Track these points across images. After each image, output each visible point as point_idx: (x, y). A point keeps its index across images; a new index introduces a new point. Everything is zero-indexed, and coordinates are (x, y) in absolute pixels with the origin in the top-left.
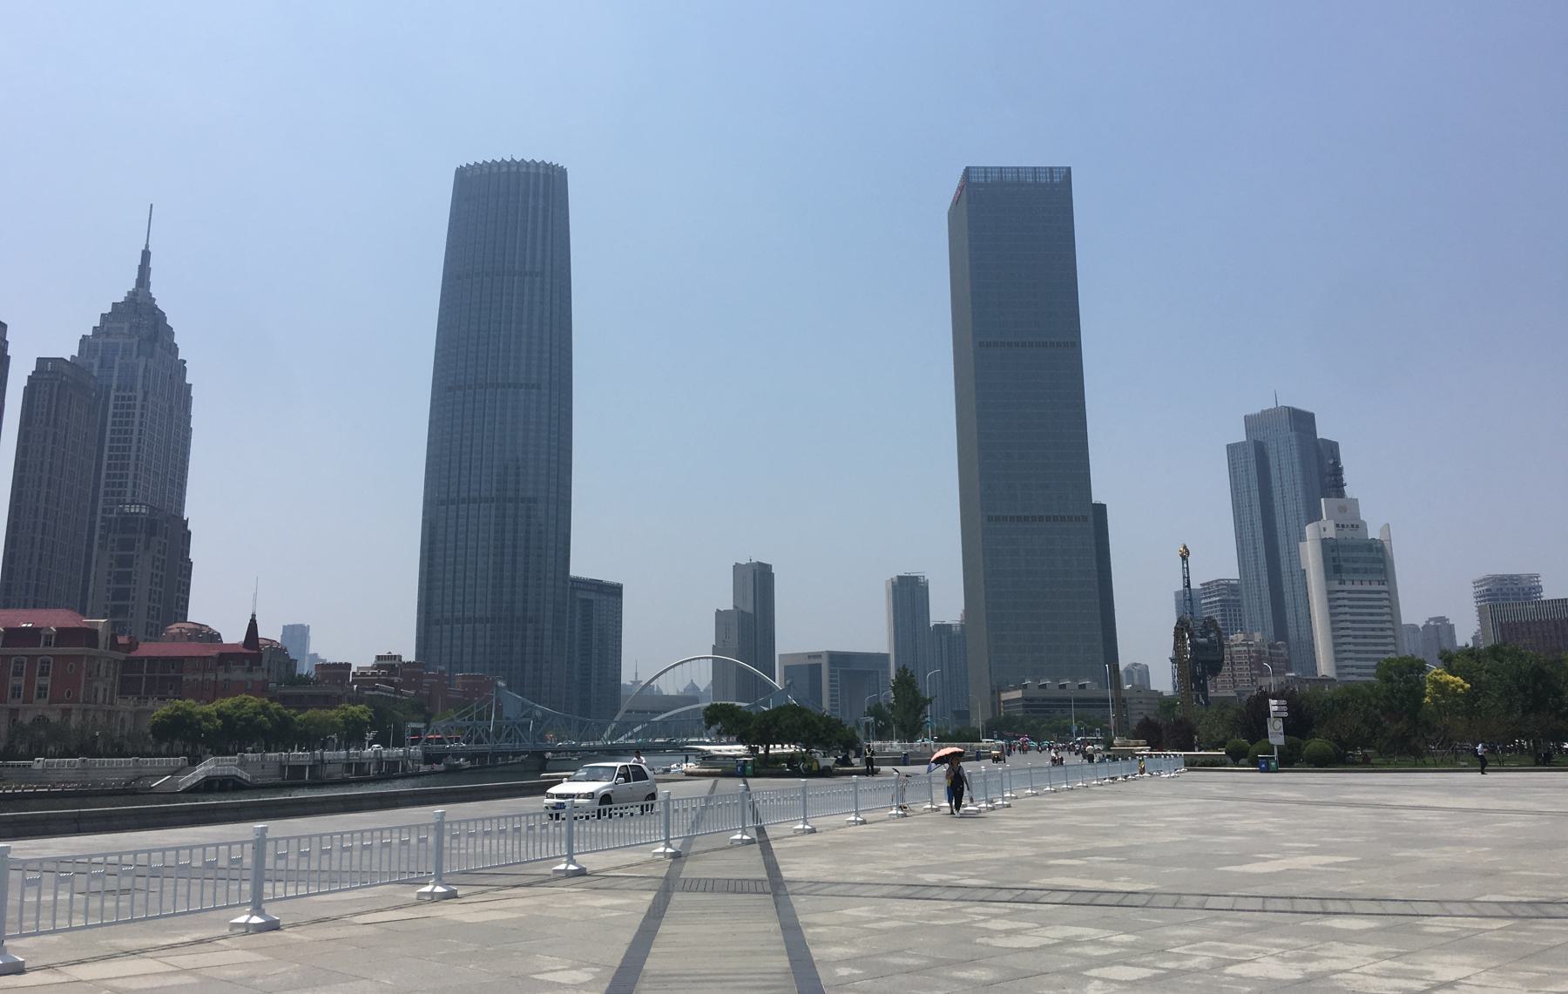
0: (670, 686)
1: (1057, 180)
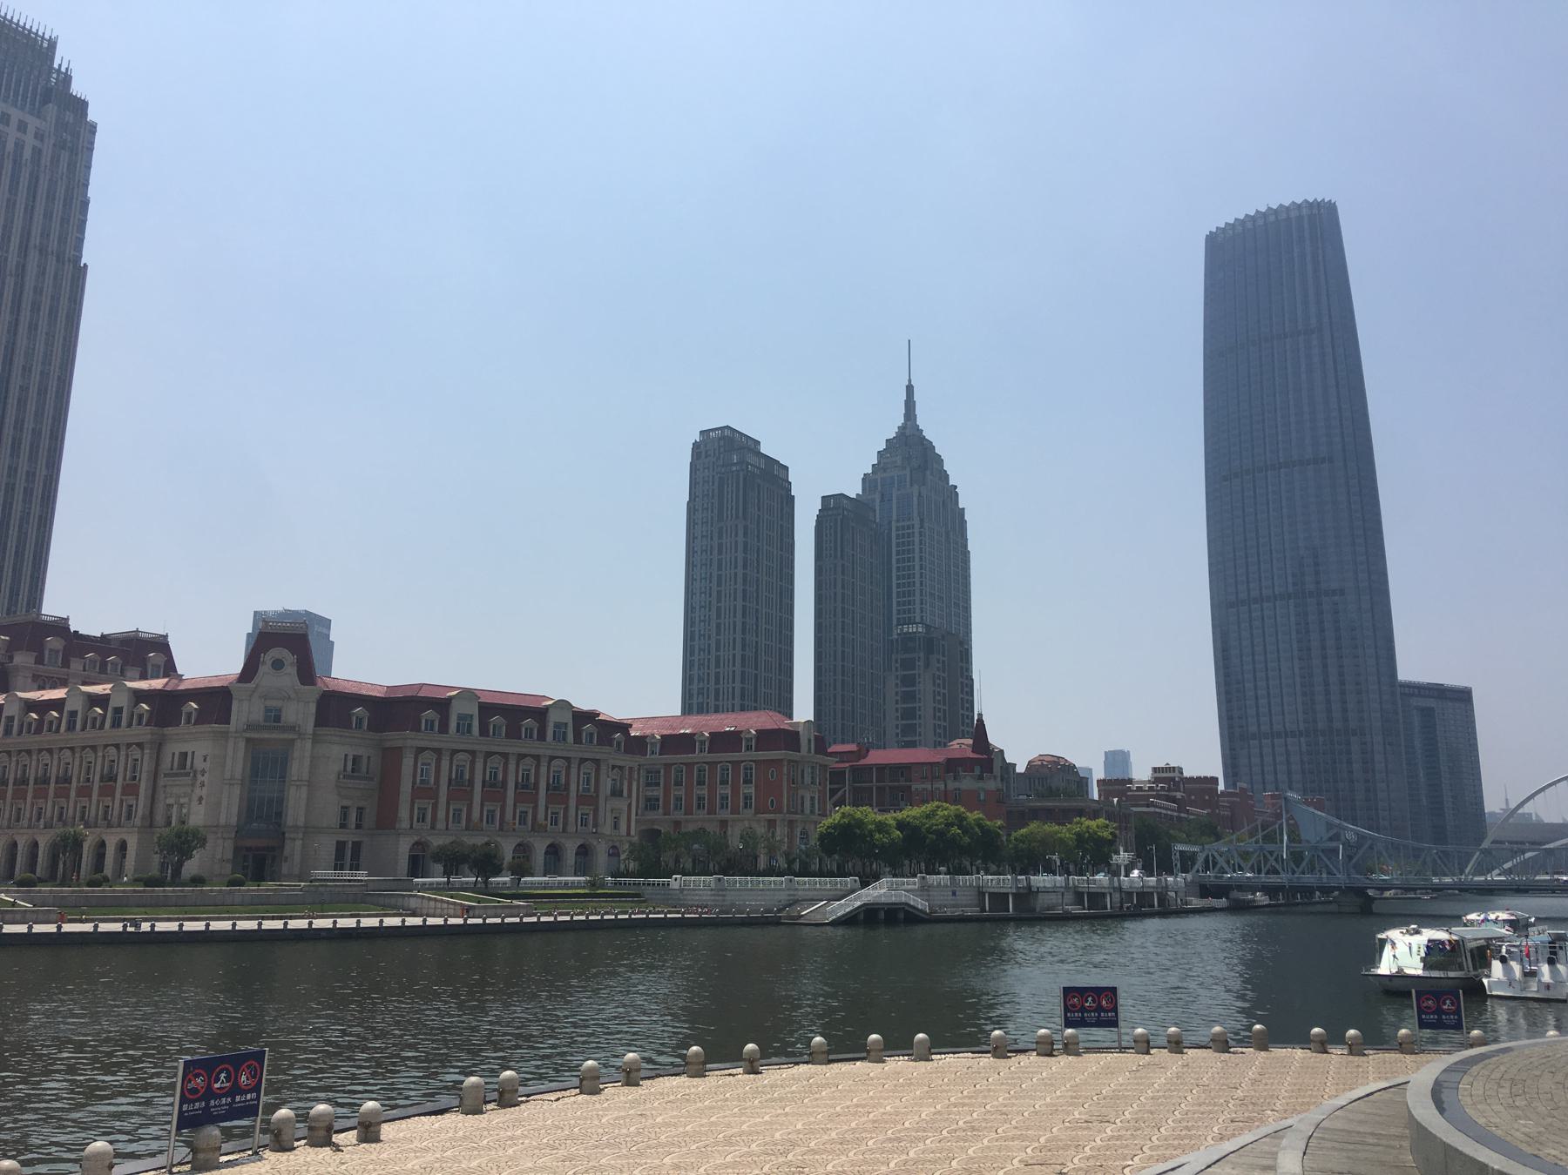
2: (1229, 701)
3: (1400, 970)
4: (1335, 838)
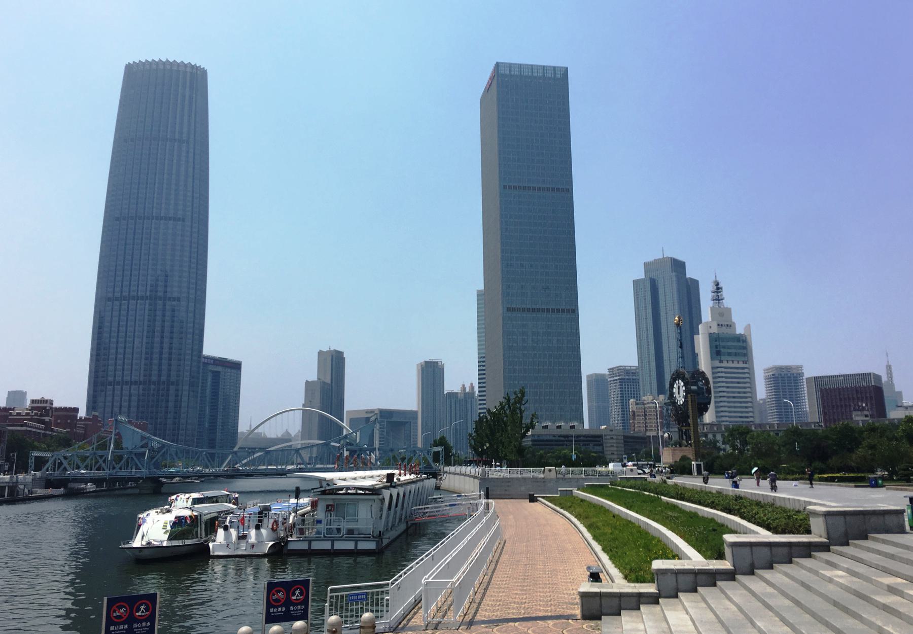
0: (272, 431)
1: (558, 76)
2: (97, 360)
3: (149, 543)
4: (145, 446)
